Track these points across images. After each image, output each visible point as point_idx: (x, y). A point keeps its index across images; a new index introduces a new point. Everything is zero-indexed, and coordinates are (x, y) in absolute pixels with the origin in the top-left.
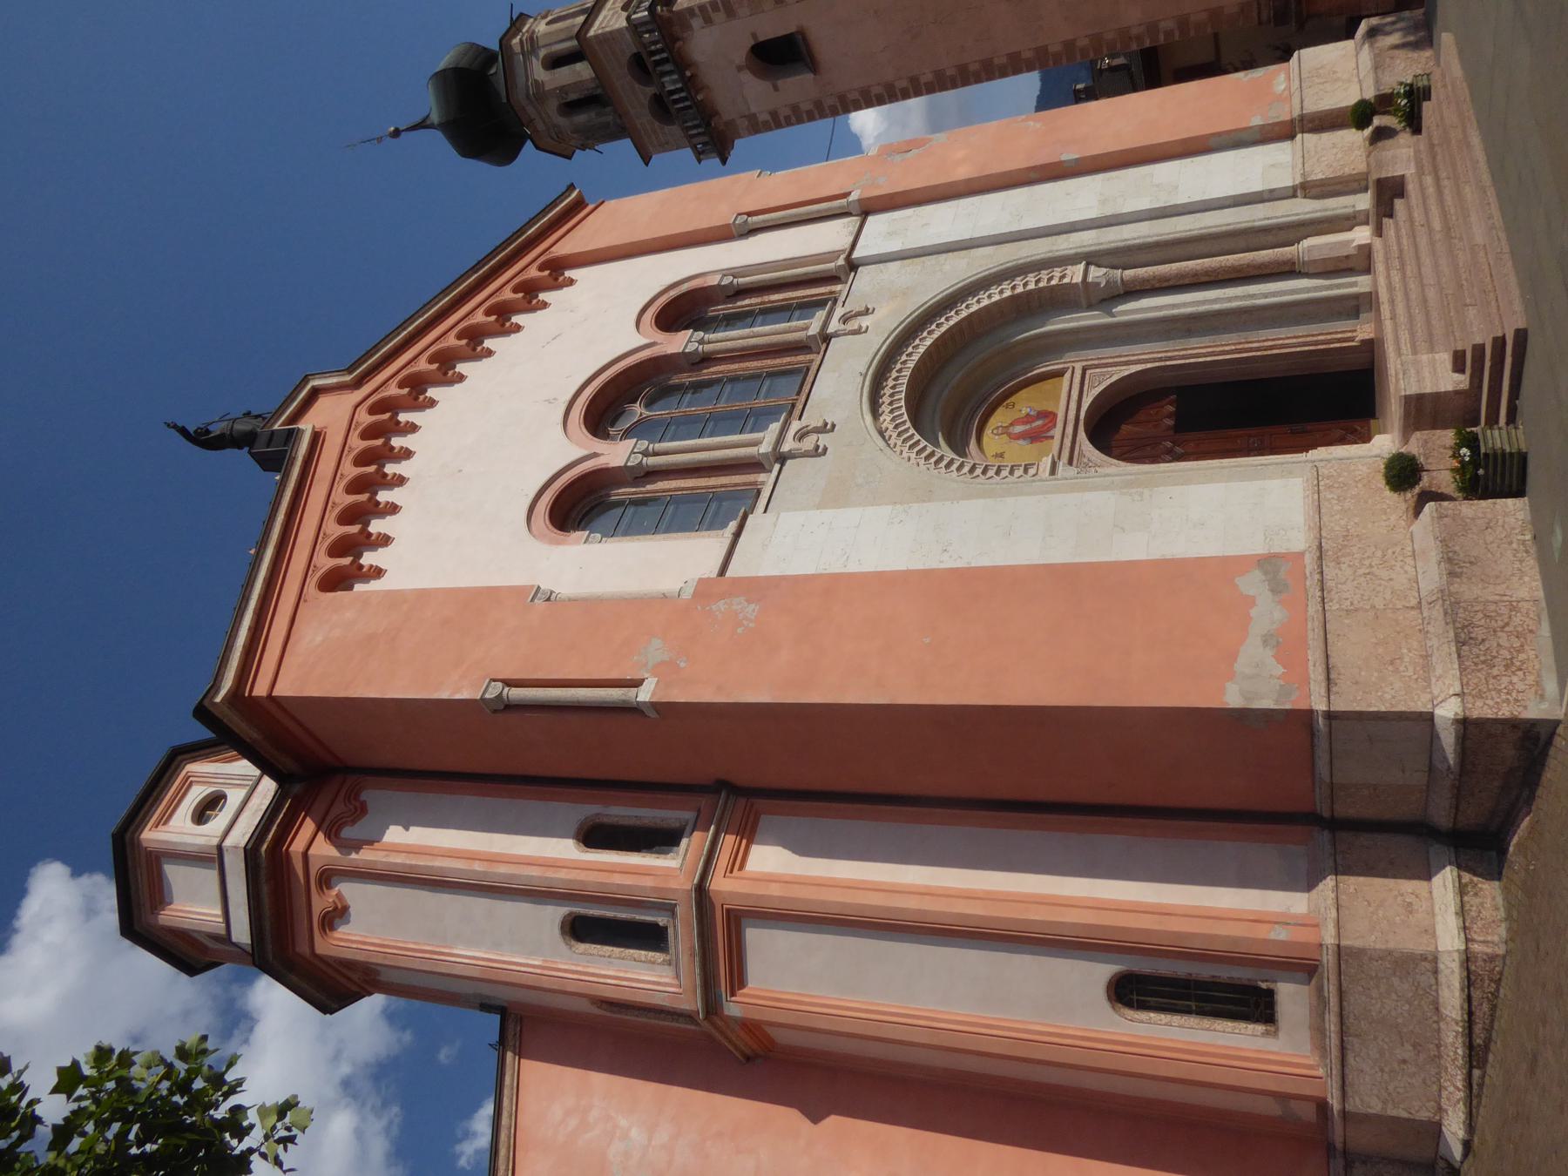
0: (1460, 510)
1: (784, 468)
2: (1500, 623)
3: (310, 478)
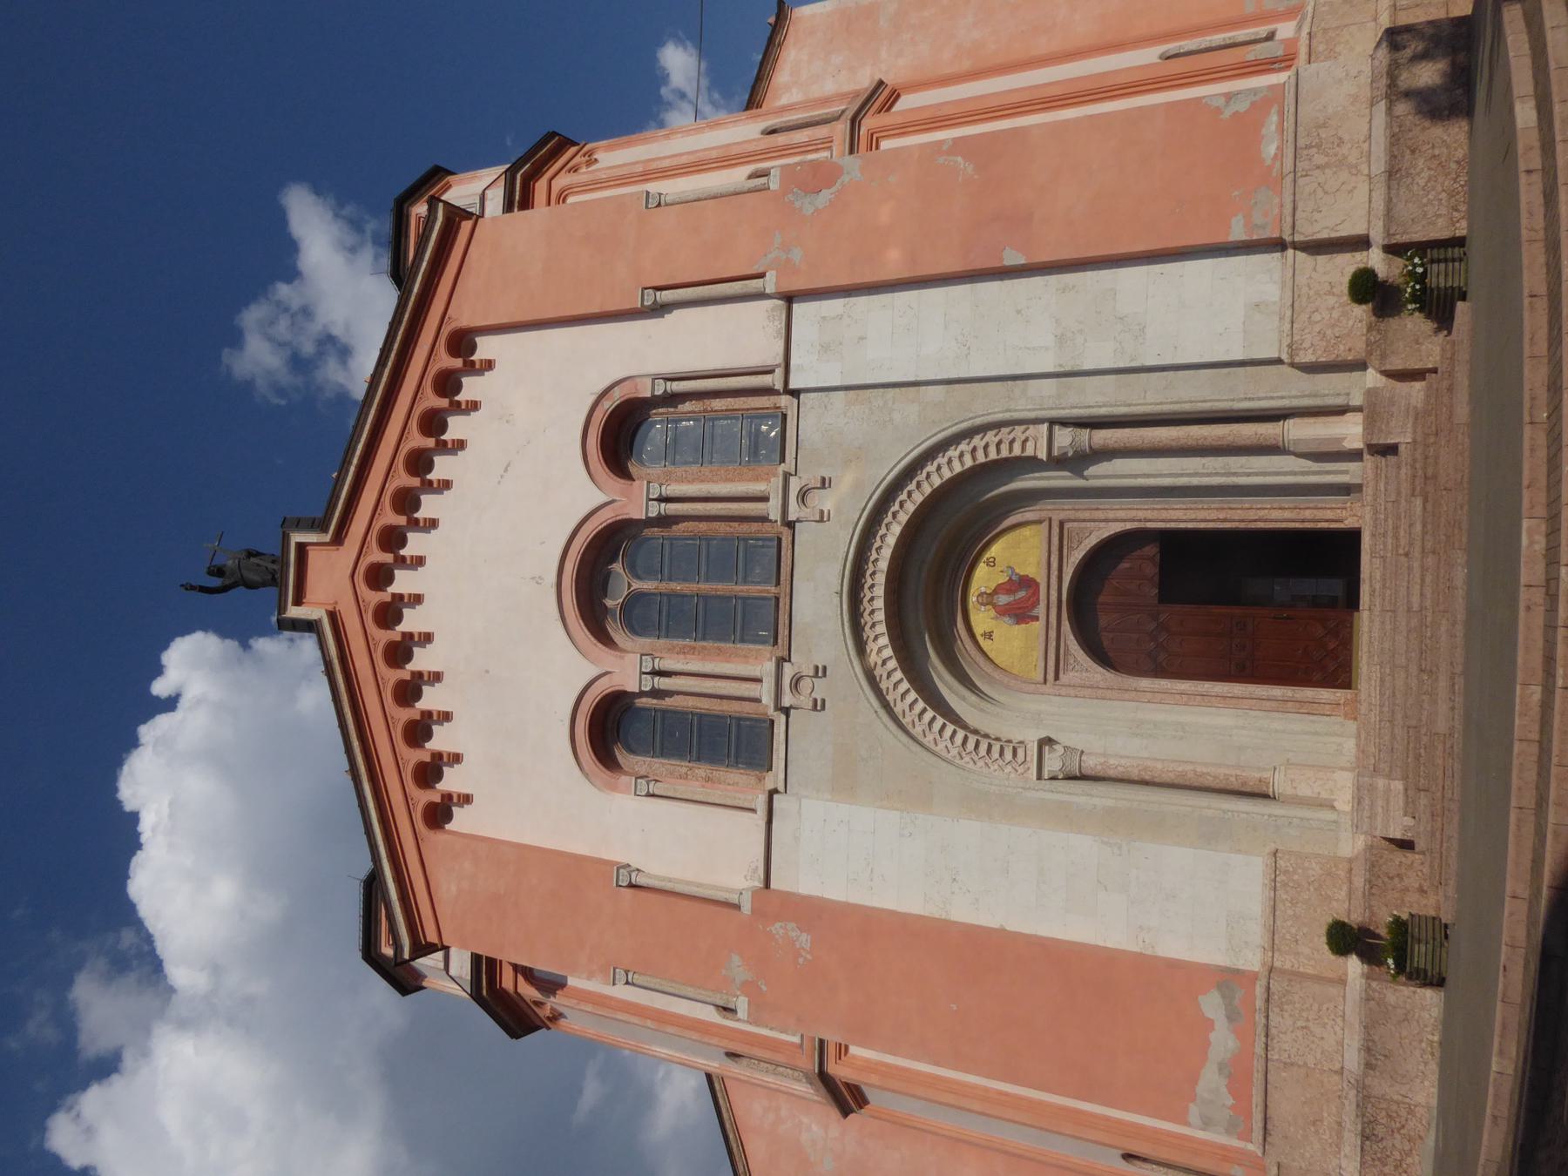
0: (1385, 995)
2: (1398, 1125)
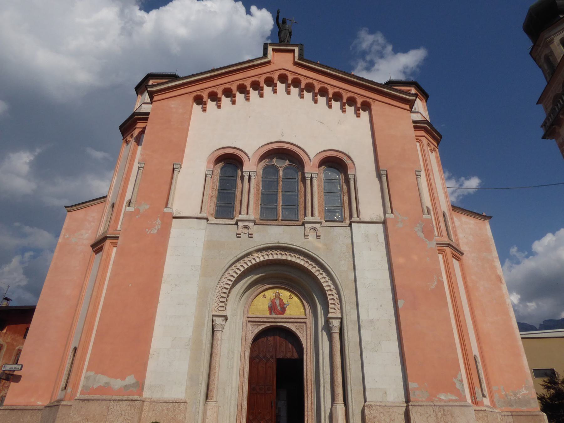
1: (233, 225)
3: (232, 74)
